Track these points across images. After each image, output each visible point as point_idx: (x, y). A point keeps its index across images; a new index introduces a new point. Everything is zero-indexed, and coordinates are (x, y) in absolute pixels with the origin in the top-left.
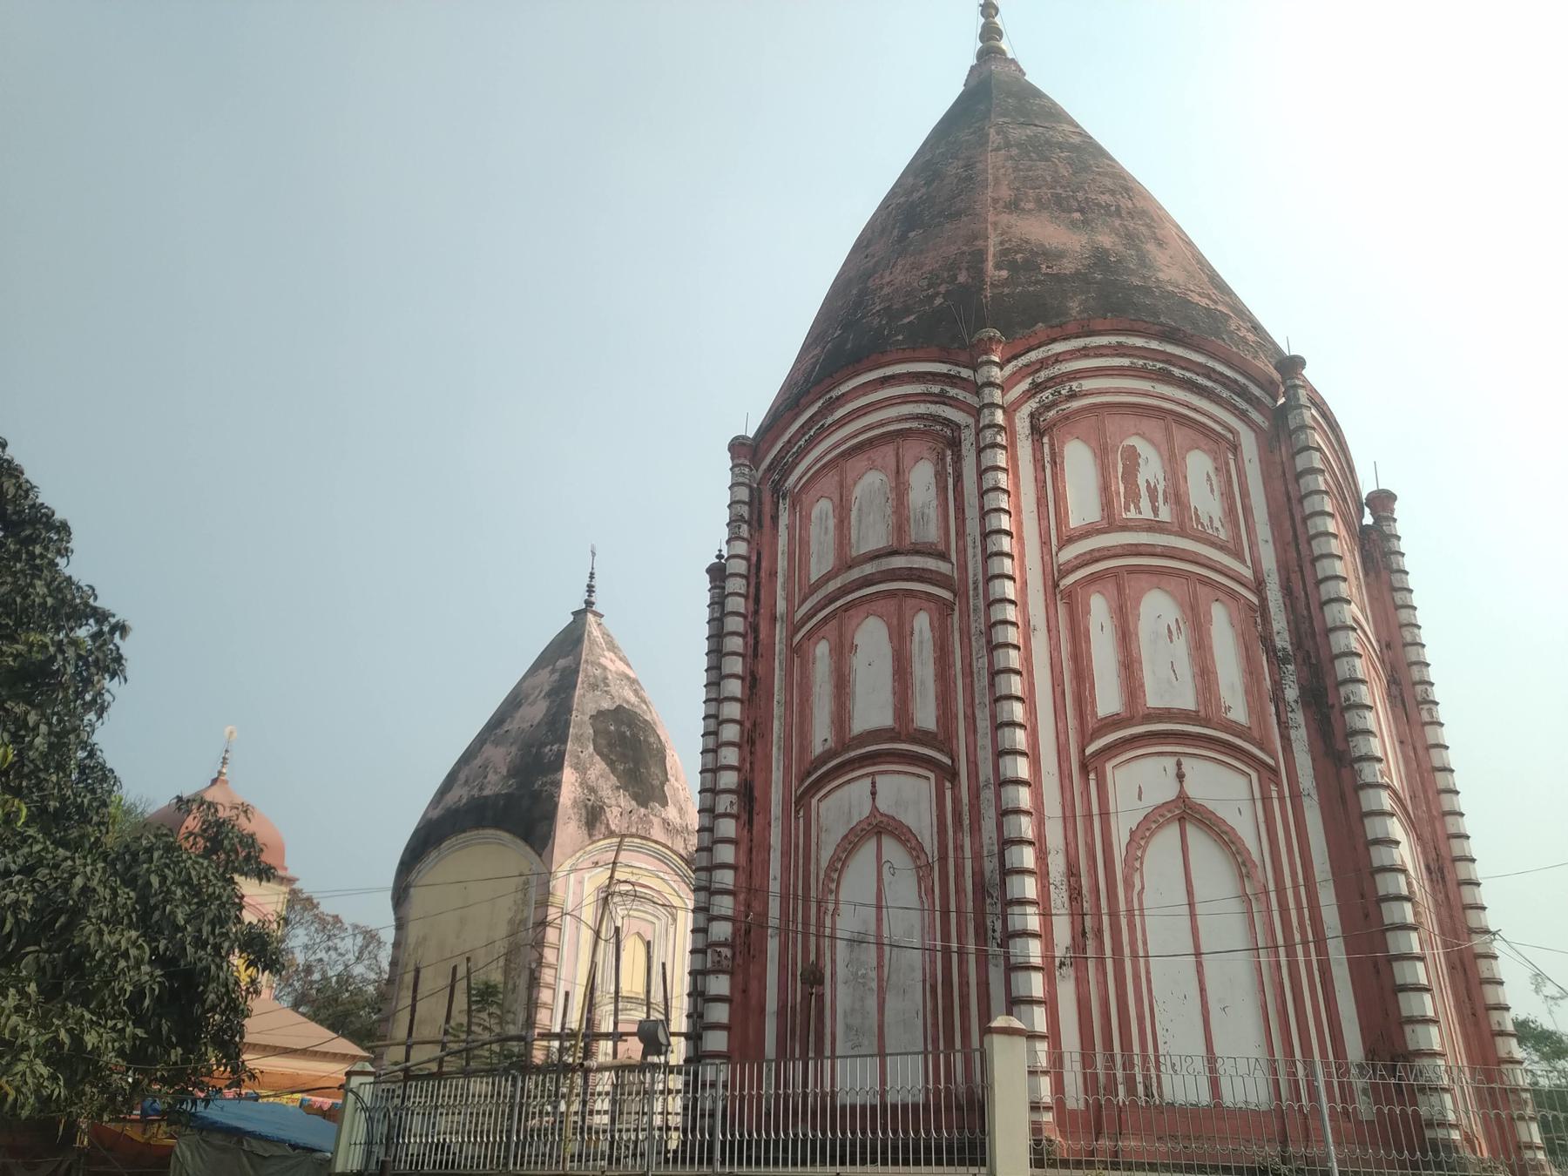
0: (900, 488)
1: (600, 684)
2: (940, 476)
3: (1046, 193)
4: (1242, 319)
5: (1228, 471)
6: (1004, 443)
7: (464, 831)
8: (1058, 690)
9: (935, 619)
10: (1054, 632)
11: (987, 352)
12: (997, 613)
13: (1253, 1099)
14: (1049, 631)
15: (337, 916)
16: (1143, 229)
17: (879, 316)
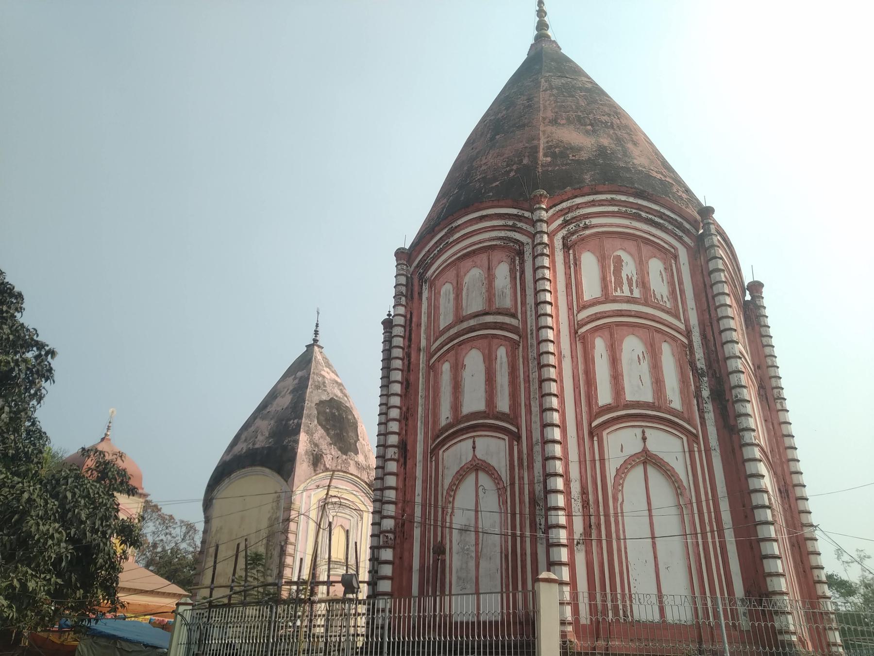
2: (512, 271)
3: (572, 115)
4: (680, 186)
5: (672, 270)
6: (548, 253)
7: (244, 468)
8: (577, 391)
10: (575, 359)
12: (544, 347)
14: (572, 358)
15: (171, 516)
17: (479, 182)
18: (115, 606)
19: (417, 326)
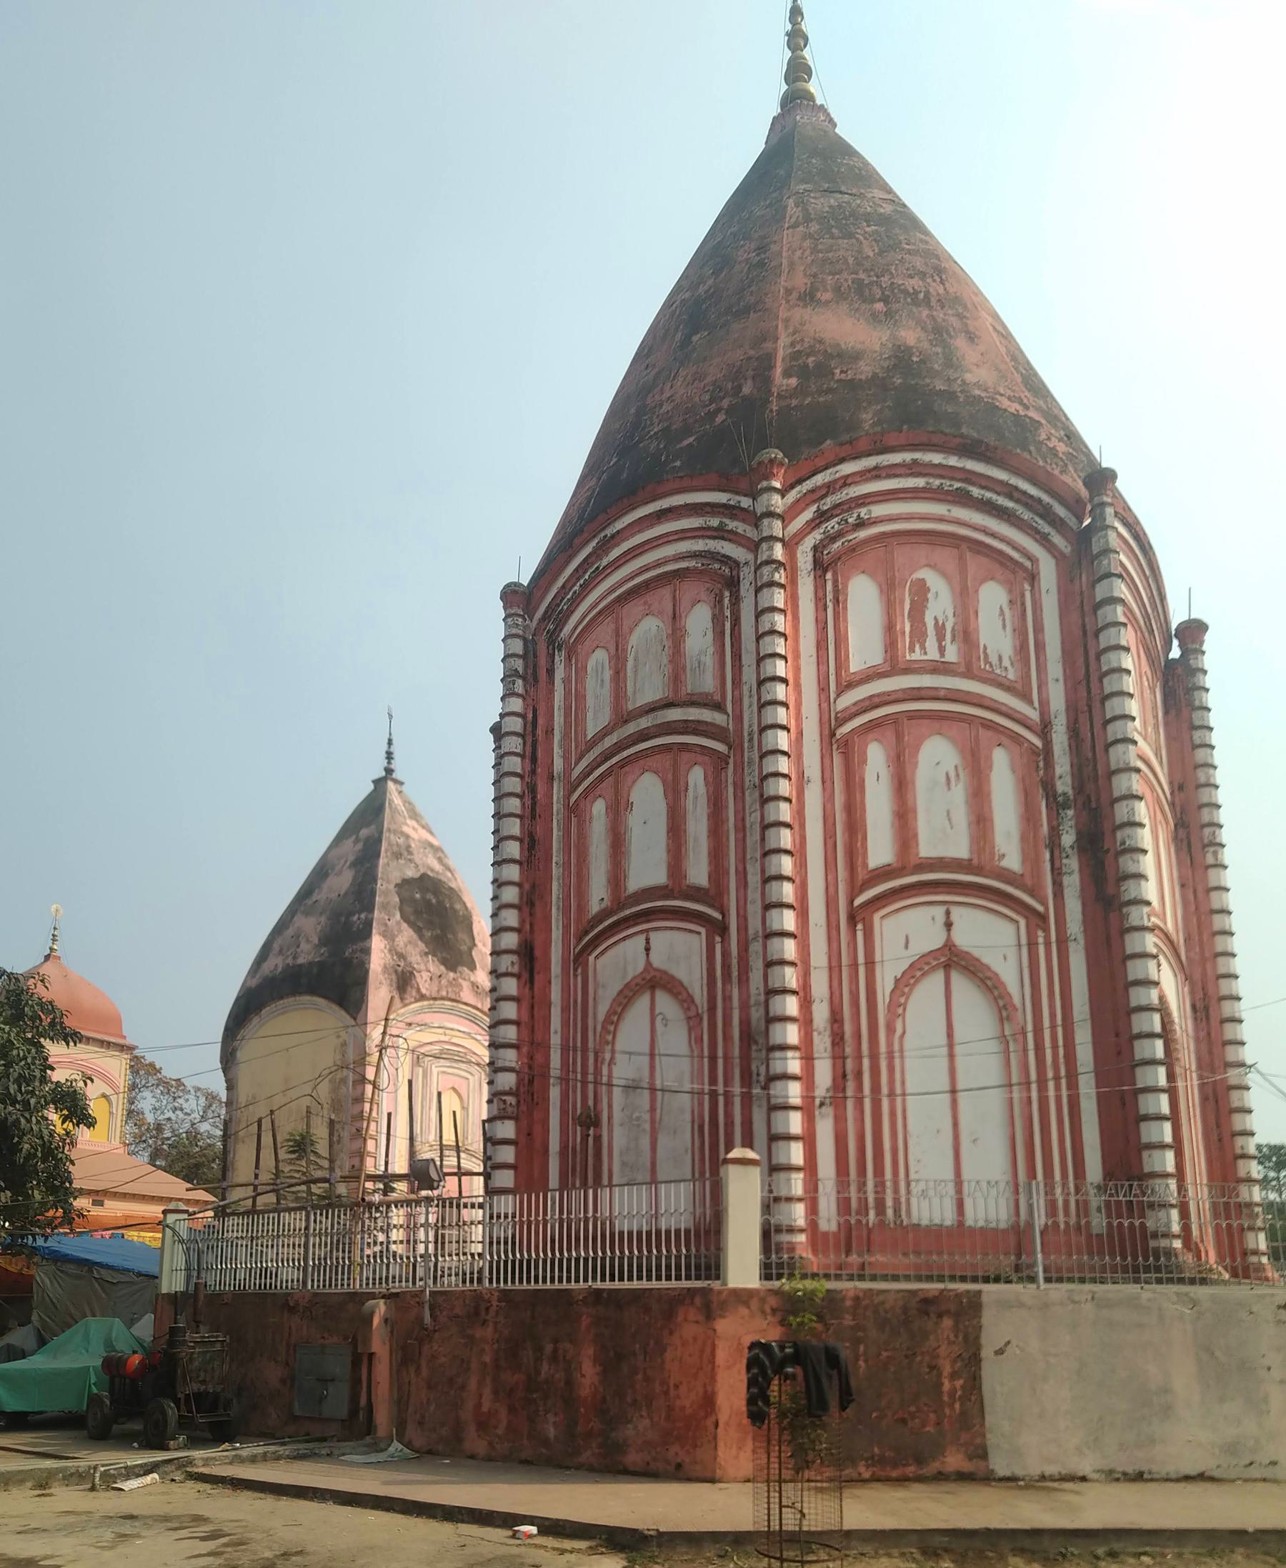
0: (677, 635)
1: (402, 853)
2: (717, 620)
3: (847, 279)
4: (1055, 427)
5: (1023, 604)
6: (783, 581)
7: (281, 998)
8: (830, 843)
9: (710, 773)
10: (828, 783)
11: (768, 477)
12: (771, 765)
13: (992, 1216)
14: (823, 782)
16: (954, 321)
17: (657, 438)
18: (69, 1218)
19: (547, 732)
